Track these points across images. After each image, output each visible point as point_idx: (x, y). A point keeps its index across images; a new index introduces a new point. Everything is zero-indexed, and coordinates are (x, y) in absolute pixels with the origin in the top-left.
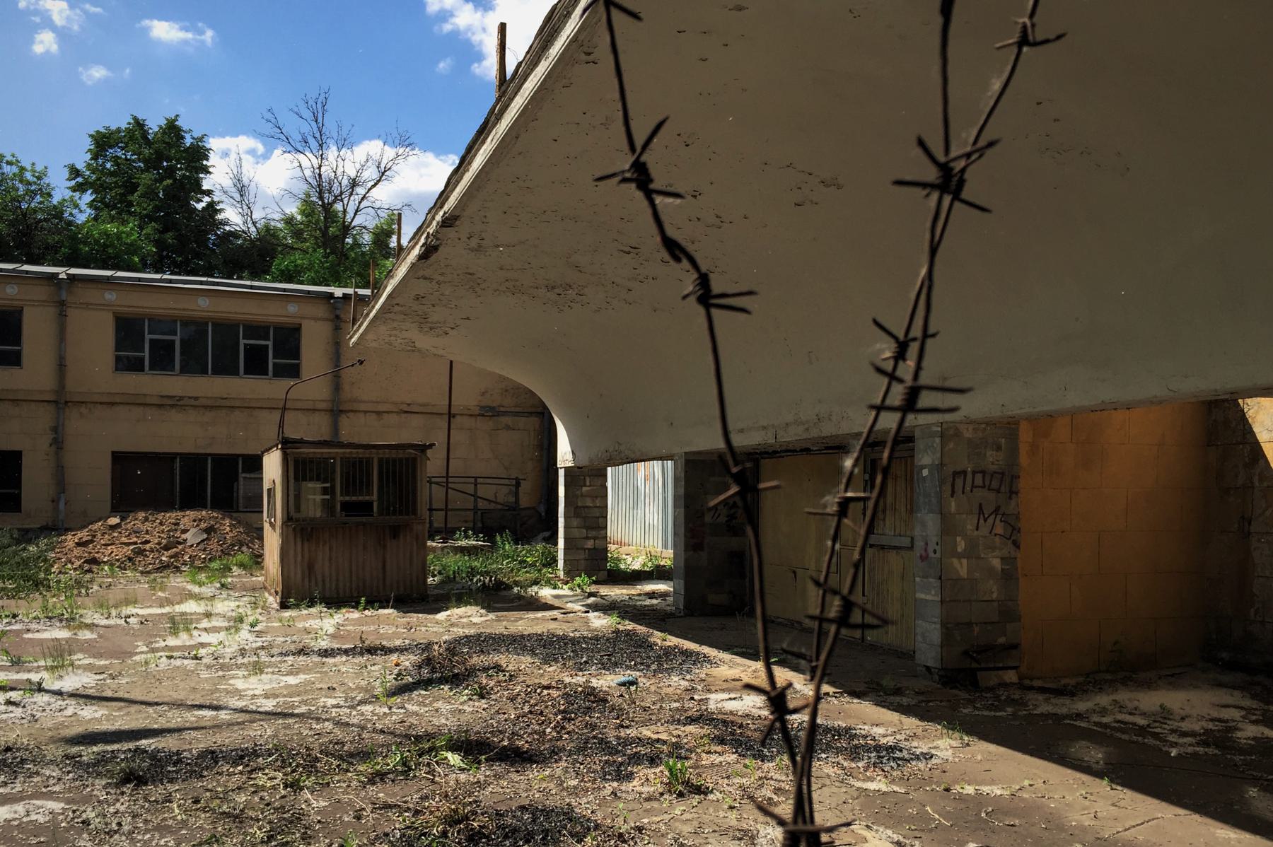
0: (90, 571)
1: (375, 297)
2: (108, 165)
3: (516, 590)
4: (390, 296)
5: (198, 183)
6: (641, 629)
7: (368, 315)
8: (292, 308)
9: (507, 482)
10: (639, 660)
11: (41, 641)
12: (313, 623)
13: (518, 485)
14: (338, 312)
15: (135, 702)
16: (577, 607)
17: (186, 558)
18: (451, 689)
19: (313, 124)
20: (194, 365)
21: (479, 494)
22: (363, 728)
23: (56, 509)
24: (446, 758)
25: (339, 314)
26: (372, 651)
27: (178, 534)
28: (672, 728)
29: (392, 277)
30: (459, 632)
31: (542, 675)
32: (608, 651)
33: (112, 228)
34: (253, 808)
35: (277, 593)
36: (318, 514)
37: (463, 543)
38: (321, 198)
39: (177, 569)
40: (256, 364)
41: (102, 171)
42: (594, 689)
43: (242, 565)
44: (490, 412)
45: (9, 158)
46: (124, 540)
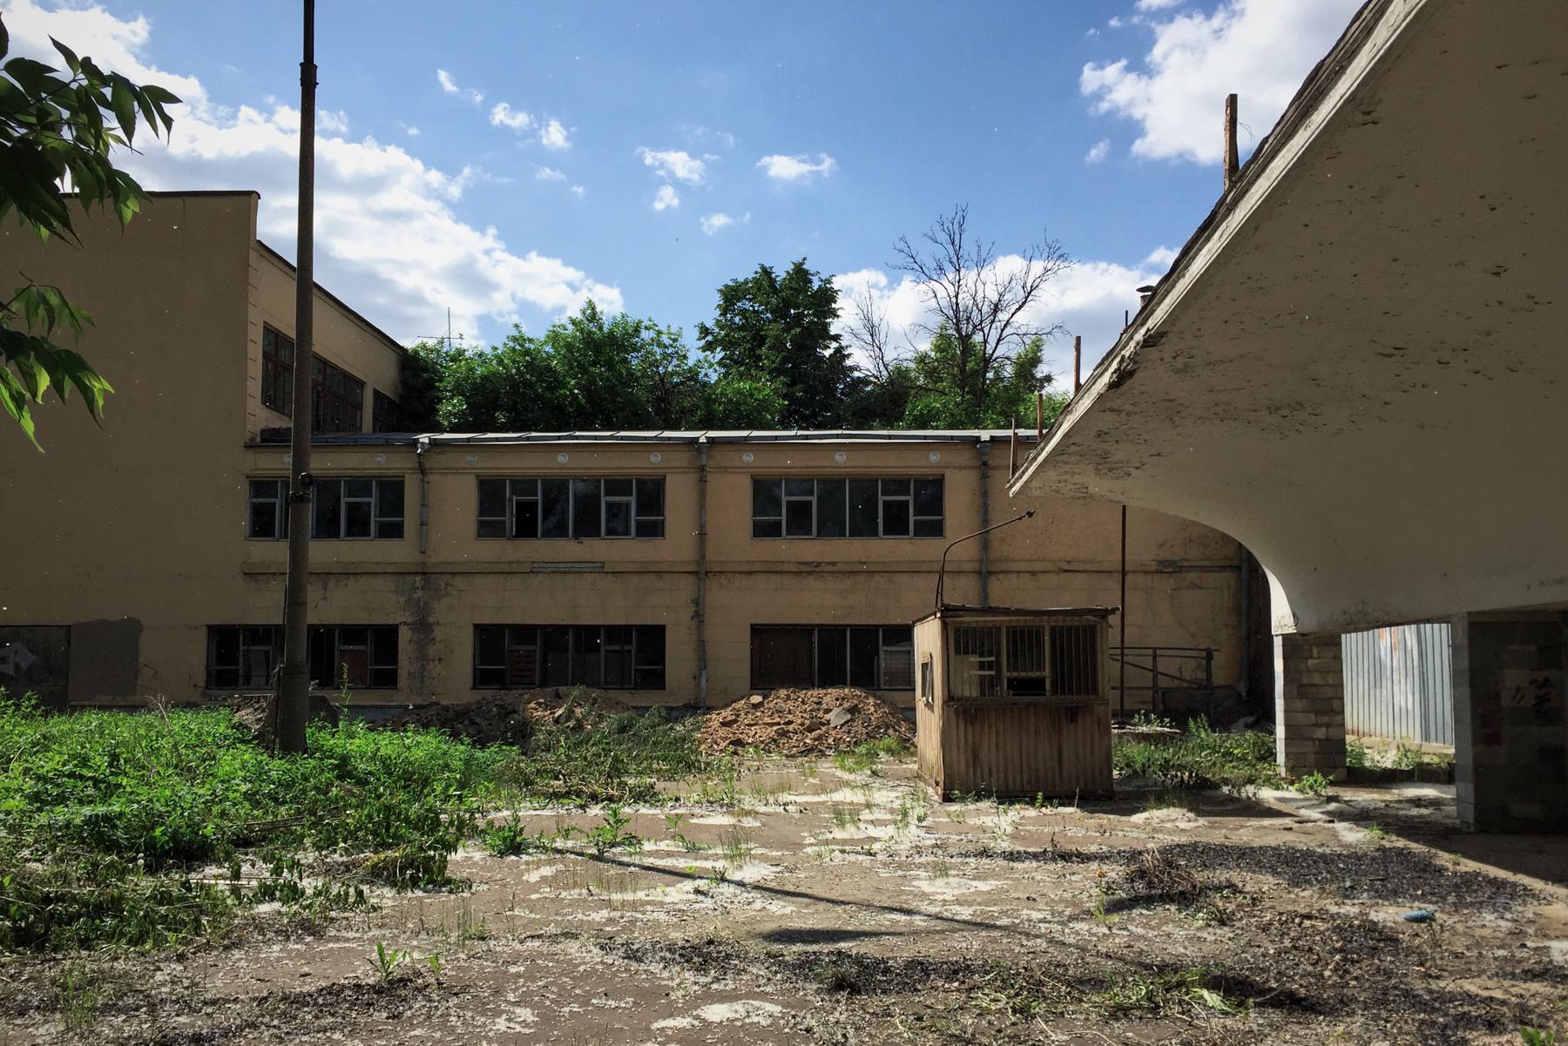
0: (735, 753)
1: (1046, 438)
2: (737, 319)
3: (1225, 789)
4: (1067, 435)
5: (826, 327)
6: (1416, 847)
7: (1035, 458)
8: (934, 457)
9: (1195, 653)
10: (1427, 888)
11: (708, 827)
12: (989, 821)
13: (1209, 655)
14: (985, 458)
15: (822, 900)
16: (1314, 814)
17: (830, 741)
18: (1180, 911)
19: (950, 247)
20: (832, 528)
21: (1160, 669)
22: (1084, 950)
23: (698, 686)
24: (1202, 997)
25: (984, 458)
26: (1066, 857)
27: (820, 714)
28: (1506, 983)
29: (1070, 412)
30: (1168, 839)
31: (1294, 901)
32: (1384, 872)
33: (745, 386)
34: (983, 1034)
35: (937, 784)
36: (975, 694)
37: (1144, 729)
38: (958, 330)
39: (822, 754)
40: (896, 525)
41: (731, 326)
42: (1376, 924)
43: (889, 751)
44: (1170, 568)
45: (646, 323)
46: (767, 720)
